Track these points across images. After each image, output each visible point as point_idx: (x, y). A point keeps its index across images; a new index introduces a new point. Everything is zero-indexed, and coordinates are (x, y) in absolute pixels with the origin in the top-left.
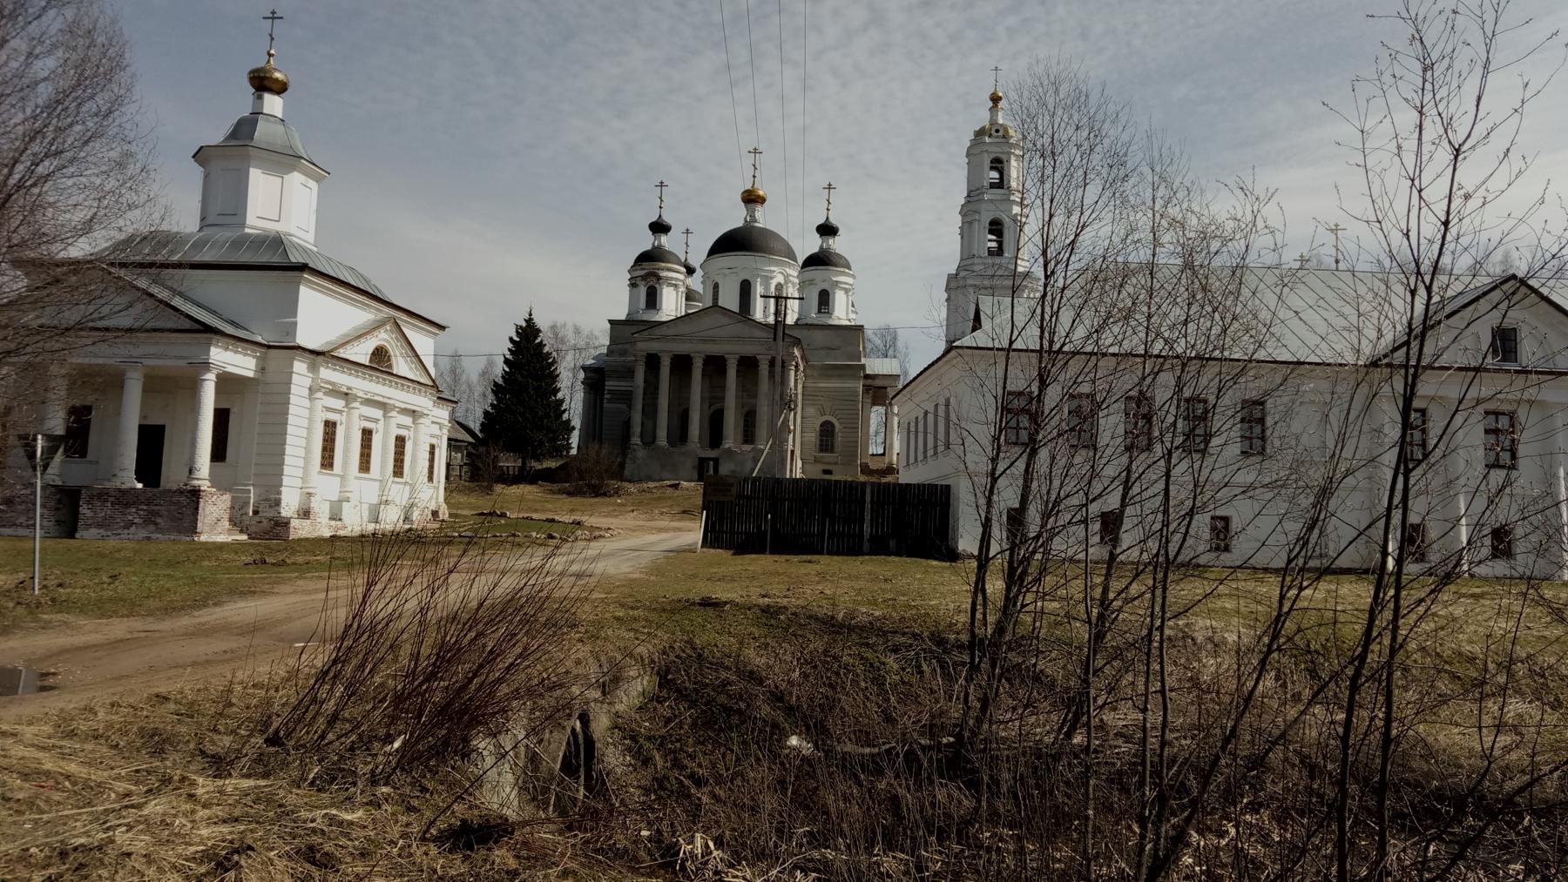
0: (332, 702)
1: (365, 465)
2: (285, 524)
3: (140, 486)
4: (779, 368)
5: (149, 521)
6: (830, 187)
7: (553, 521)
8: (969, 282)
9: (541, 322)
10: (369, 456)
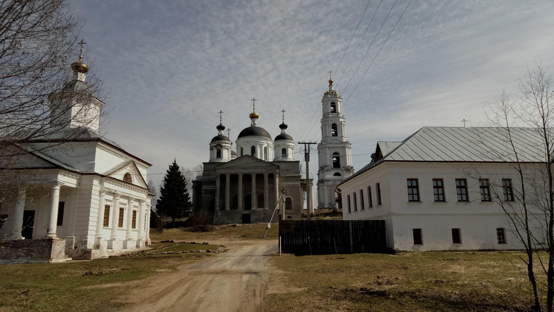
0: (17, 284)
1: (121, 225)
2: (89, 252)
3: (24, 238)
4: (272, 177)
5: (28, 254)
6: (283, 111)
7: (194, 243)
8: (327, 146)
9: (178, 163)
10: (122, 219)
